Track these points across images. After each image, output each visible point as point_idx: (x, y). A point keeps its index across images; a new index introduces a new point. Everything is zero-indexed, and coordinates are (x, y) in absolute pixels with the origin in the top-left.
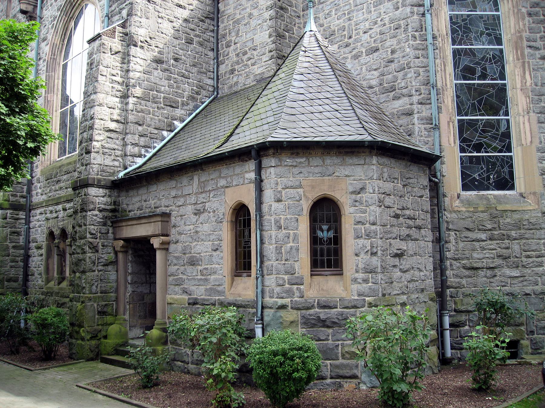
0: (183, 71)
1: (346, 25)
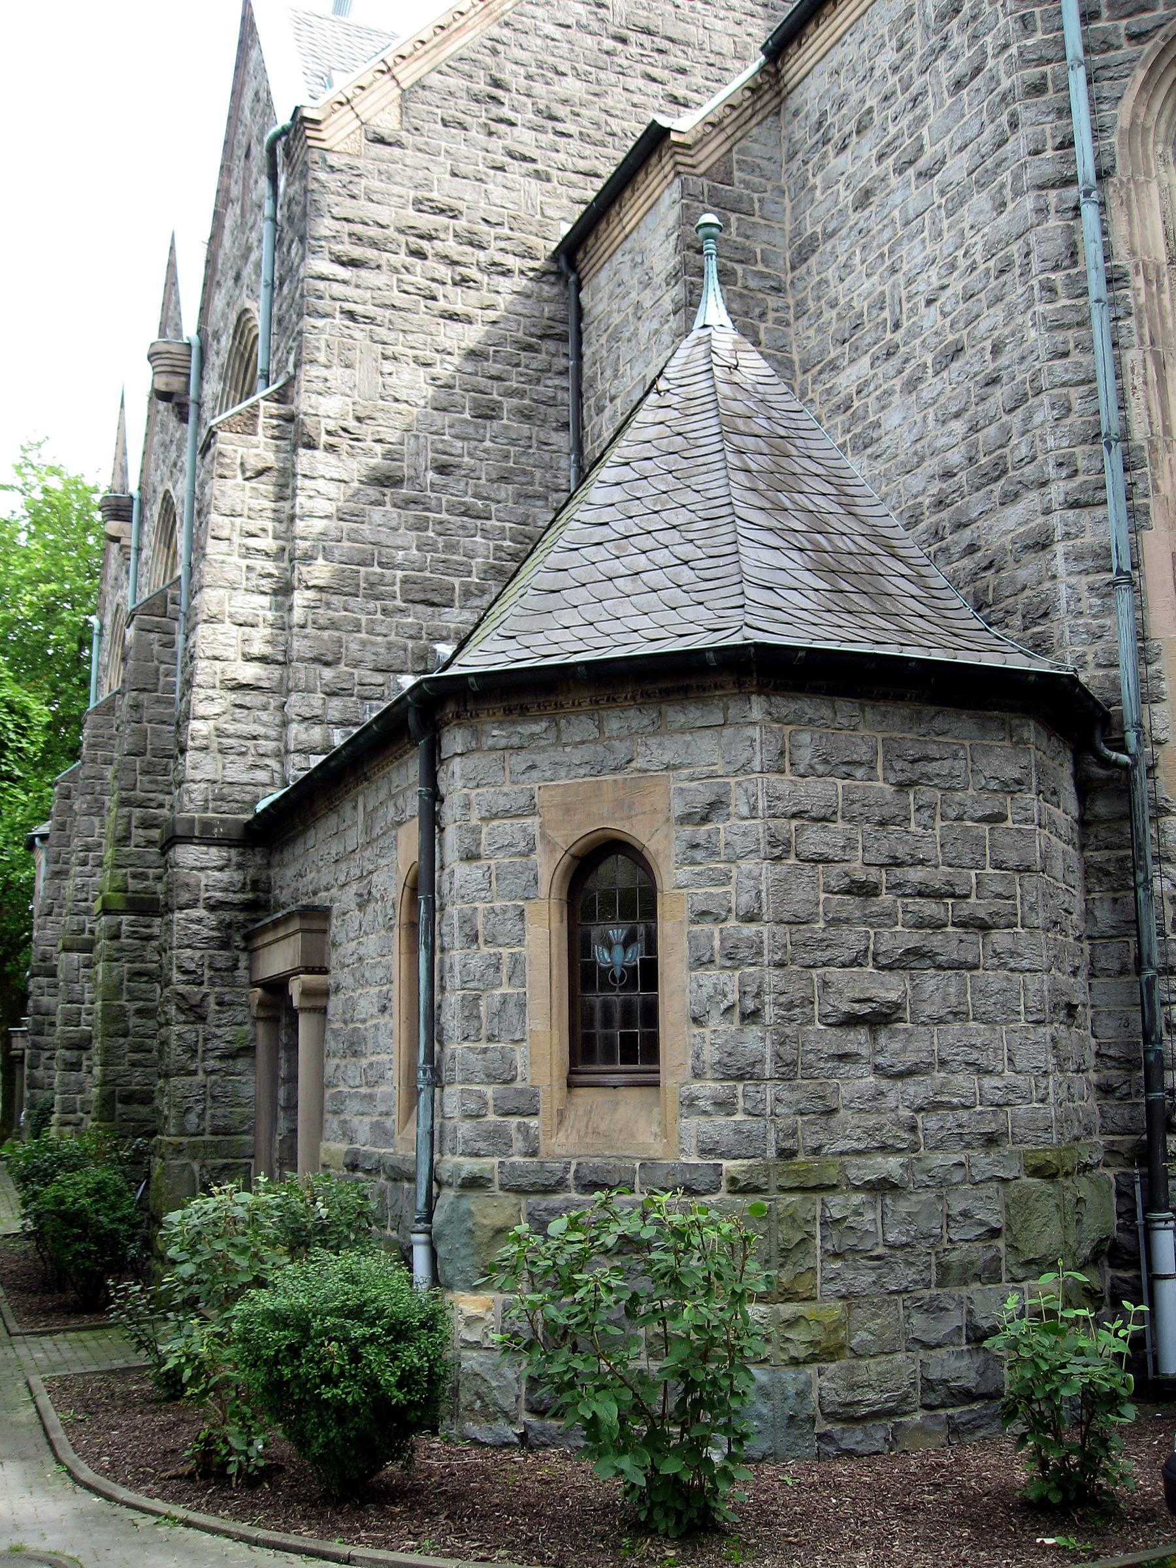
0: (468, 499)
1: (886, 288)
